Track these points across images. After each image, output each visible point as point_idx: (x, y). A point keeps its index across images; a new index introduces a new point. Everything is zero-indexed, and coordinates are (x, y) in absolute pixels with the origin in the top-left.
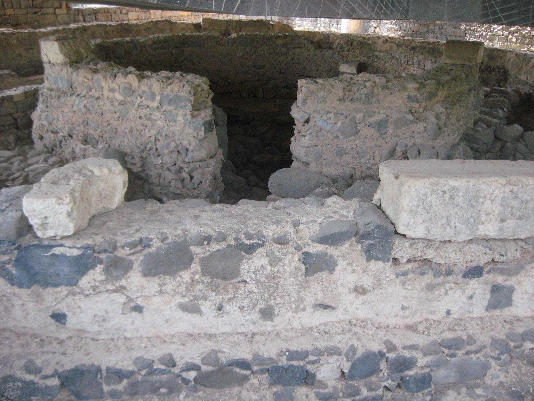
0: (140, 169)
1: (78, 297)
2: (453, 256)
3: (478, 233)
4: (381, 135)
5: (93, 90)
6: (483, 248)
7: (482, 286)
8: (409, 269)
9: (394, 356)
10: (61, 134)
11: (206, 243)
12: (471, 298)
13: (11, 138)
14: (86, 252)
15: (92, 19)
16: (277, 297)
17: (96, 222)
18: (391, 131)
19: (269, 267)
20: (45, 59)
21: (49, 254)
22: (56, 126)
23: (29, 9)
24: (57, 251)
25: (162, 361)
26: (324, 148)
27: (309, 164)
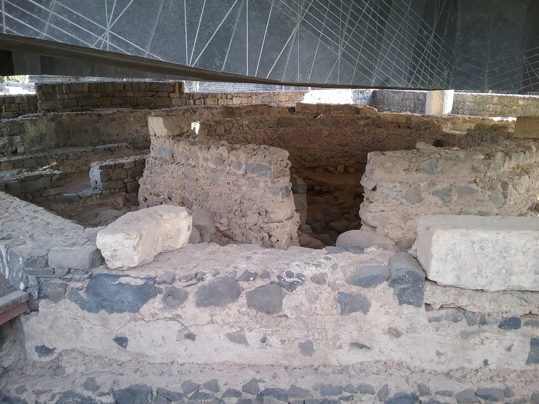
0: (226, 228)
1: (140, 322)
2: (487, 305)
3: (511, 284)
4: (444, 203)
5: (191, 159)
6: (518, 299)
7: (521, 338)
8: (442, 315)
9: (427, 400)
10: (162, 196)
11: (251, 279)
12: (509, 349)
13: (120, 200)
14: (149, 282)
15: (201, 102)
16: (315, 333)
17: (161, 258)
18: (455, 198)
19: (307, 304)
20: (151, 132)
21: (117, 282)
22: (158, 190)
23: (147, 93)
24: (123, 280)
25: (206, 385)
26: (390, 213)
27: (376, 228)
